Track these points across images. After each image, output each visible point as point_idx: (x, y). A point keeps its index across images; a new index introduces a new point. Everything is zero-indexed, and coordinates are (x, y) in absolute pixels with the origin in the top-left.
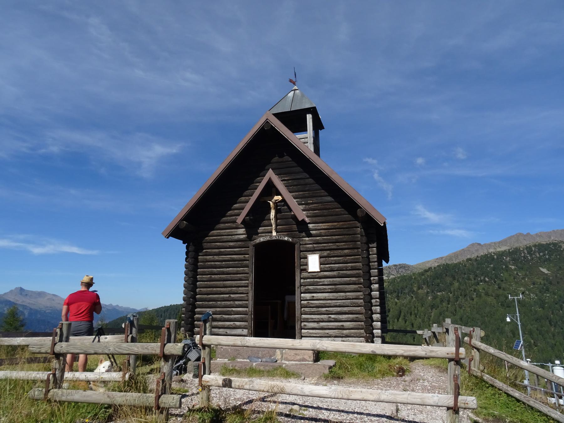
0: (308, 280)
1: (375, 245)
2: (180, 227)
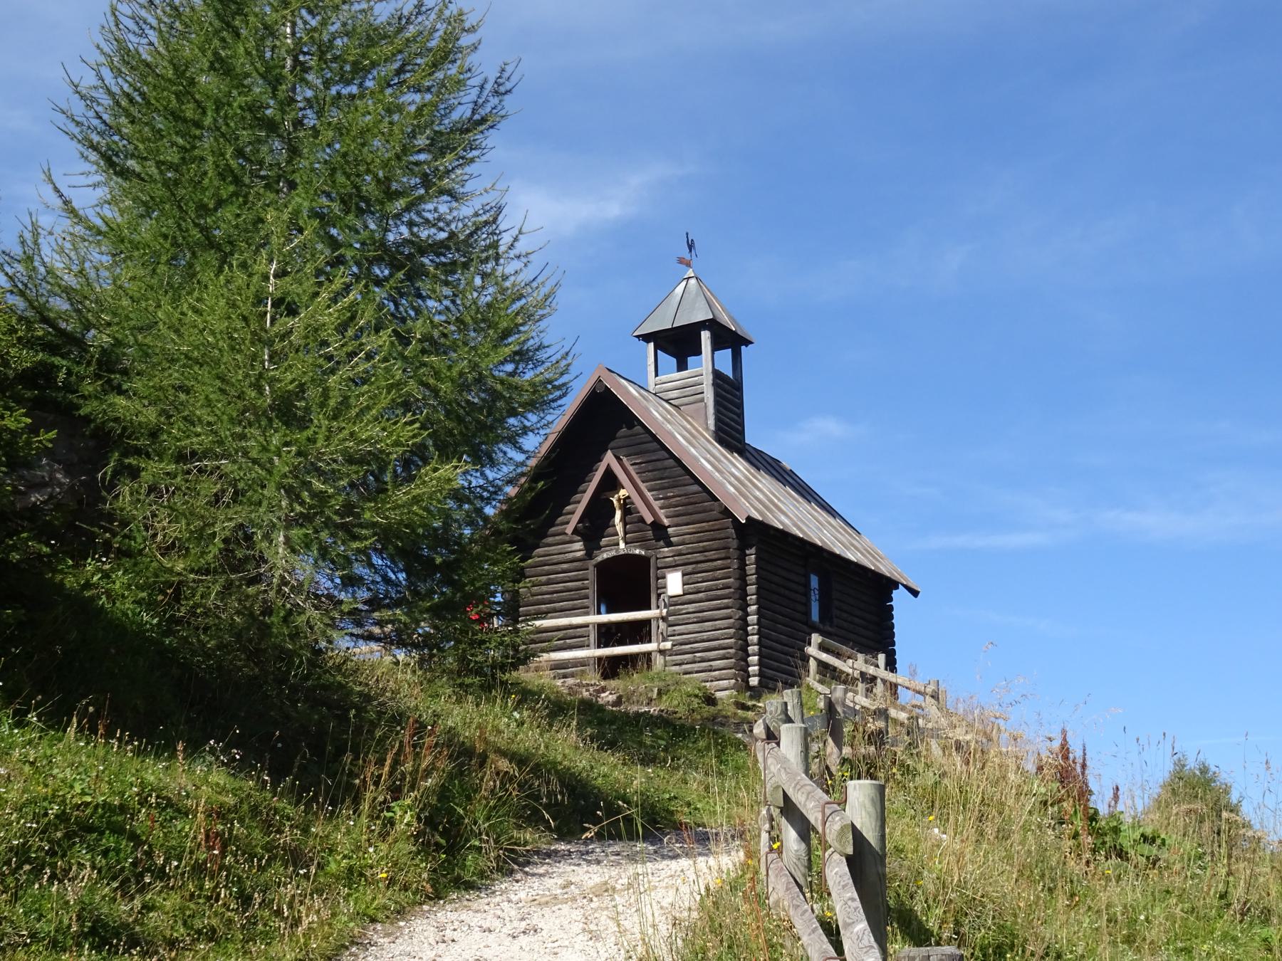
1: (753, 550)
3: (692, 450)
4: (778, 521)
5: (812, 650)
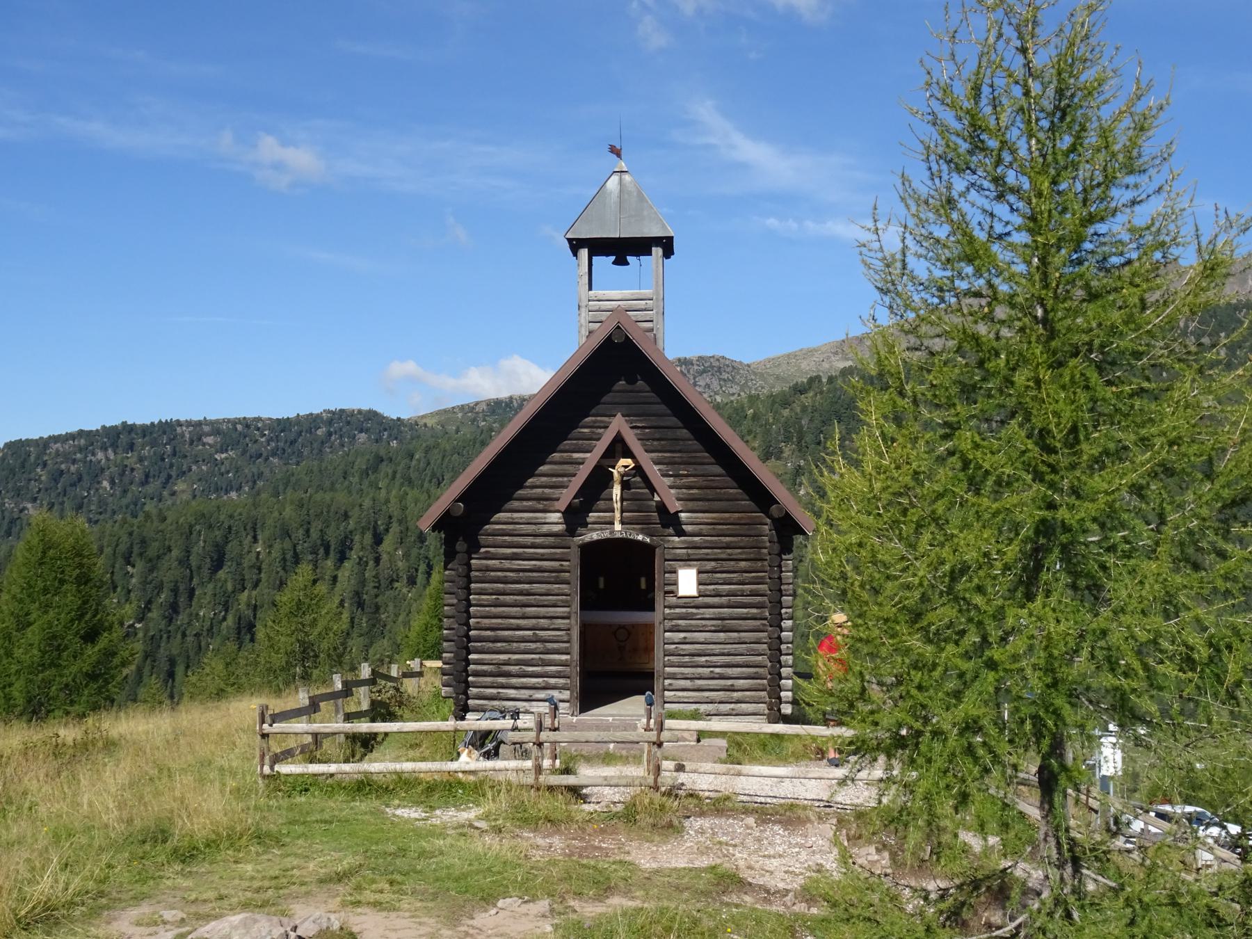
0: (678, 610)
2: (452, 514)
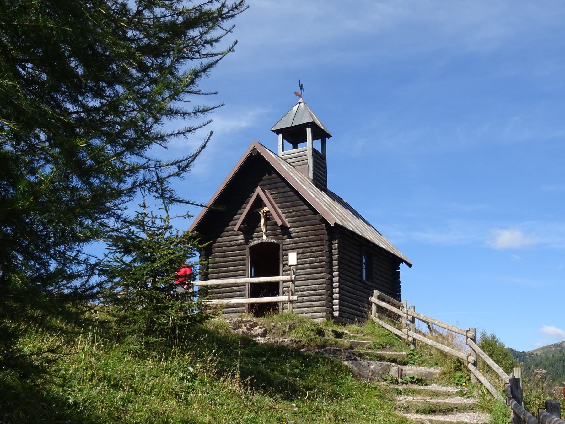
1: (336, 242)
3: (304, 187)
4: (350, 227)
5: (374, 299)
